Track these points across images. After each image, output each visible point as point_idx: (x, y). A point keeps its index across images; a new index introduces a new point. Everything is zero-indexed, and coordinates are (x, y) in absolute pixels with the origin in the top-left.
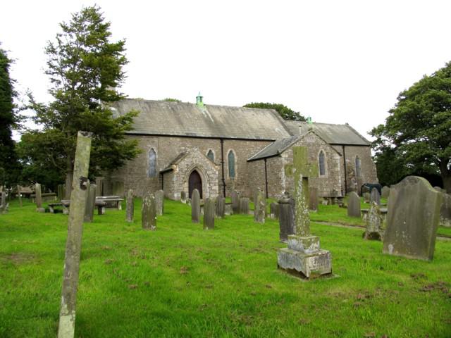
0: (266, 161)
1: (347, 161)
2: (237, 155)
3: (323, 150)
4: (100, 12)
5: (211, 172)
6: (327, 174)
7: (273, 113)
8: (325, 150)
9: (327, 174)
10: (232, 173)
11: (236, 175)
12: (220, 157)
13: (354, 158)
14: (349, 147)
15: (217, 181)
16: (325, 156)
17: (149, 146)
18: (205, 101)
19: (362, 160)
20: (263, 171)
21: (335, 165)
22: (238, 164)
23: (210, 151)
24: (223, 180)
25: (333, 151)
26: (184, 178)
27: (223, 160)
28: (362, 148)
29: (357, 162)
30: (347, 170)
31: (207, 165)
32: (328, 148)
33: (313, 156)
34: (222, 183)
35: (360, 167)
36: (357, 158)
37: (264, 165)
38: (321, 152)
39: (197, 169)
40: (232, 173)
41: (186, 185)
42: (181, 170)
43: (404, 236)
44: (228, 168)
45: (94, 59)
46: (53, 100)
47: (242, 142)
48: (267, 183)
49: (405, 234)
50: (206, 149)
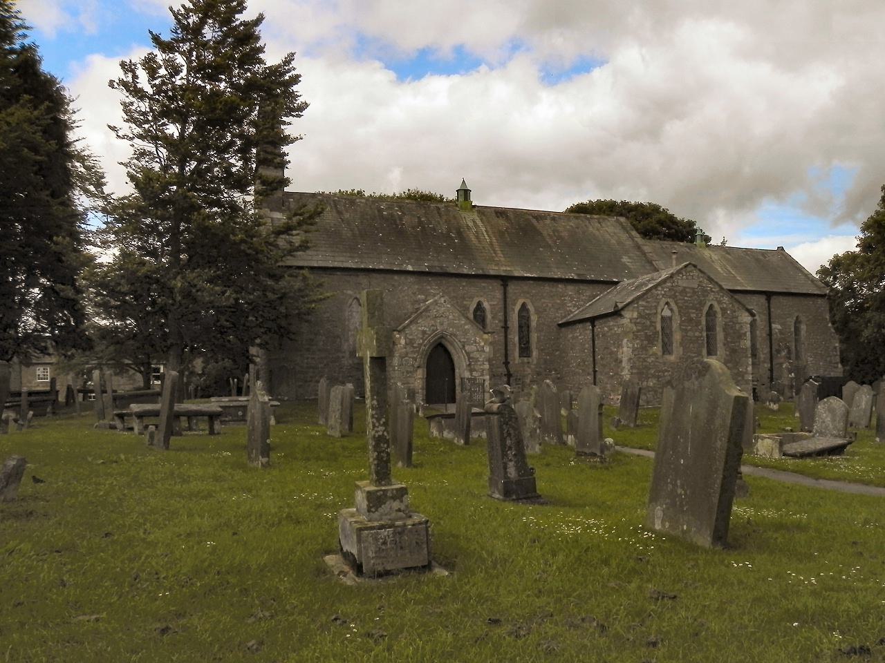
0: (593, 326)
1: (776, 327)
2: (537, 312)
3: (715, 304)
4: (74, 117)
7: (621, 224)
8: (719, 302)
10: (525, 350)
11: (535, 353)
13: (791, 322)
14: (781, 299)
15: (487, 366)
16: (719, 315)
17: (349, 292)
20: (588, 346)
21: (741, 336)
23: (479, 304)
24: (506, 363)
25: (736, 305)
26: (415, 359)
27: (506, 321)
28: (810, 302)
29: (797, 330)
30: (775, 347)
31: (465, 332)
32: (726, 299)
34: (503, 370)
36: (798, 322)
37: (589, 333)
38: (711, 307)
39: (444, 342)
40: (525, 350)
41: (420, 374)
42: (410, 343)
43: (679, 491)
44: (517, 339)
45: (225, 95)
47: (547, 287)
49: (682, 487)
50: (472, 298)
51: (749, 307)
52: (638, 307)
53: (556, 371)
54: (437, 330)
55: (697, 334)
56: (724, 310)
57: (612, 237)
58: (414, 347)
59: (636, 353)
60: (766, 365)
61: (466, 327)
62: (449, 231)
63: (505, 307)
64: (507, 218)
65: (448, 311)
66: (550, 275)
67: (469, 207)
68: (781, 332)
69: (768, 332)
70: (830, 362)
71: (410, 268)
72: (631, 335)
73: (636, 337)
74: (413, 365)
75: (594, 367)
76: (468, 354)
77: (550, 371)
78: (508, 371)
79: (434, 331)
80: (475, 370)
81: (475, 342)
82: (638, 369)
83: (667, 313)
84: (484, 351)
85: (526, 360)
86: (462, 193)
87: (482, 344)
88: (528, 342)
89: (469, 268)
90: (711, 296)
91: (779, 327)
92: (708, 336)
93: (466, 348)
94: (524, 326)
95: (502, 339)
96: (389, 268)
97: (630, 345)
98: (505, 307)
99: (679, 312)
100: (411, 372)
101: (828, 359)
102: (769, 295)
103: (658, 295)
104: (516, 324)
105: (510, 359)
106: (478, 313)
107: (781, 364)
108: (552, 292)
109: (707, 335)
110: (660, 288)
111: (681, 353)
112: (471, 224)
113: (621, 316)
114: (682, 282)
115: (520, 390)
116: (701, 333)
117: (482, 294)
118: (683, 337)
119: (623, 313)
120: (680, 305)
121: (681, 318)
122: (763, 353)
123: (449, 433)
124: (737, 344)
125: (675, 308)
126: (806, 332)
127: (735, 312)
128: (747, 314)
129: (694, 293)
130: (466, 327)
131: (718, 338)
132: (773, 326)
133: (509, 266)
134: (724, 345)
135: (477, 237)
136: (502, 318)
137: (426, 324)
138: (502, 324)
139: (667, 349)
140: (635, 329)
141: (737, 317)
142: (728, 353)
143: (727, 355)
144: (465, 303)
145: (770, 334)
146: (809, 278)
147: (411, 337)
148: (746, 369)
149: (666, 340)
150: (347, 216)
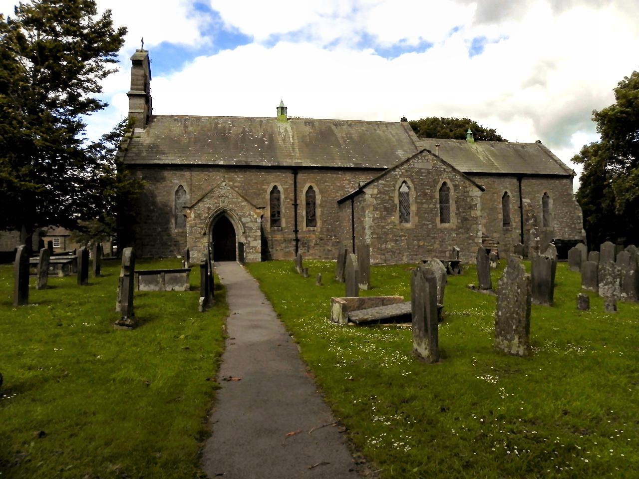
0: (353, 202)
1: (526, 201)
2: (321, 192)
3: (448, 181)
5: (248, 219)
6: (454, 222)
8: (452, 180)
9: (454, 222)
10: (311, 221)
11: (319, 223)
12: (292, 195)
18: (290, 113)
19: (554, 200)
22: (321, 206)
23: (275, 187)
24: (296, 231)
26: (202, 228)
27: (296, 200)
29: (545, 204)
30: (525, 217)
31: (242, 208)
33: (428, 191)
35: (550, 211)
38: (445, 184)
40: (311, 221)
42: (198, 216)
44: (304, 213)
46: (600, 135)
48: (354, 237)
50: (269, 183)
51: (479, 184)
52: (378, 185)
53: (335, 236)
54: (219, 206)
55: (431, 206)
56: (456, 186)
57: (394, 136)
58: (201, 220)
59: (376, 221)
60: (517, 231)
61: (243, 204)
62: (264, 136)
63: (295, 190)
64: (313, 125)
65: (228, 192)
66: (331, 165)
67: (285, 119)
68: (530, 205)
69: (519, 205)
70: (575, 227)
71: (222, 163)
72: (372, 208)
73: (376, 209)
74: (200, 233)
75: (353, 234)
76: (244, 224)
77: (331, 237)
78: (297, 237)
79: (217, 207)
80: (249, 236)
81: (250, 215)
82: (377, 234)
83: (404, 189)
84: (256, 222)
85: (312, 228)
86: (280, 109)
87: (255, 216)
88: (314, 215)
89: (268, 162)
90: (445, 175)
91: (528, 201)
92: (441, 208)
93: (242, 220)
94: (311, 204)
95: (293, 213)
96: (205, 163)
97: (371, 215)
98: (295, 190)
99: (415, 188)
100: (199, 238)
101: (573, 226)
102: (520, 177)
103: (396, 175)
104: (304, 203)
105: (298, 228)
106: (275, 195)
107: (529, 230)
108: (333, 177)
109: (440, 206)
110: (397, 170)
111: (417, 221)
112: (282, 131)
113: (364, 193)
114: (418, 164)
115: (306, 251)
116: (435, 205)
117: (277, 180)
118: (418, 208)
119: (365, 190)
120: (416, 183)
121: (417, 193)
122: (515, 220)
123: (145, 287)
124: (468, 213)
125: (411, 185)
126: (553, 205)
127: (466, 187)
128: (477, 189)
129: (429, 173)
130: (243, 204)
131: (451, 209)
132: (524, 200)
133: (301, 159)
134: (456, 214)
135: (284, 140)
136: (293, 198)
137: (211, 203)
138: (293, 202)
139: (404, 218)
140: (375, 202)
141: (468, 192)
142: (460, 221)
143: (458, 222)
144: (264, 187)
145: (521, 207)
146: (557, 163)
147: (199, 212)
148: (477, 234)
149: (403, 211)
150: (190, 129)
